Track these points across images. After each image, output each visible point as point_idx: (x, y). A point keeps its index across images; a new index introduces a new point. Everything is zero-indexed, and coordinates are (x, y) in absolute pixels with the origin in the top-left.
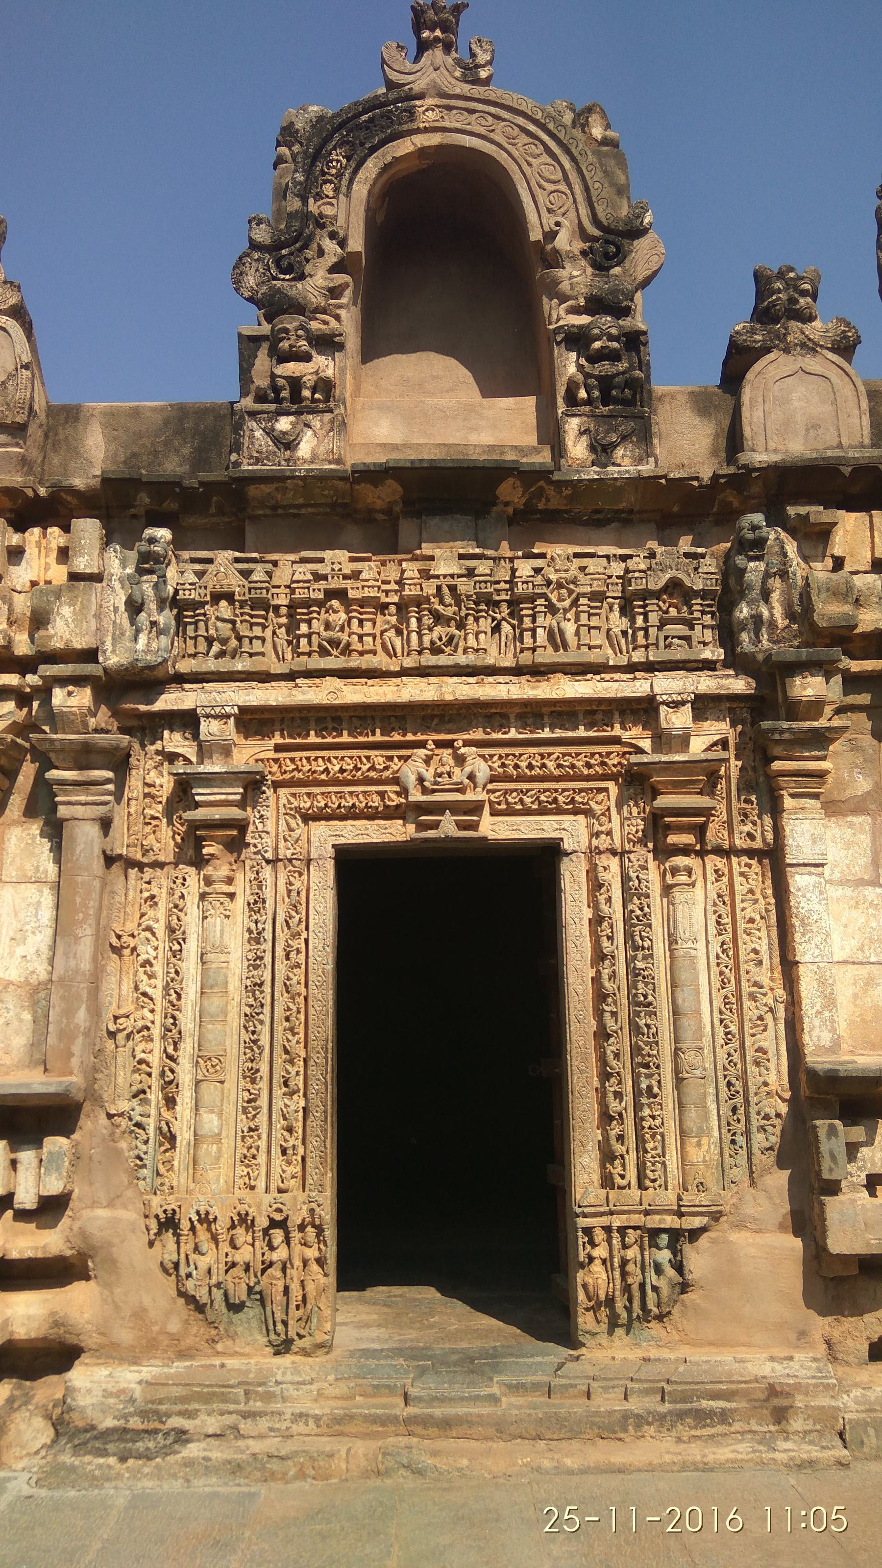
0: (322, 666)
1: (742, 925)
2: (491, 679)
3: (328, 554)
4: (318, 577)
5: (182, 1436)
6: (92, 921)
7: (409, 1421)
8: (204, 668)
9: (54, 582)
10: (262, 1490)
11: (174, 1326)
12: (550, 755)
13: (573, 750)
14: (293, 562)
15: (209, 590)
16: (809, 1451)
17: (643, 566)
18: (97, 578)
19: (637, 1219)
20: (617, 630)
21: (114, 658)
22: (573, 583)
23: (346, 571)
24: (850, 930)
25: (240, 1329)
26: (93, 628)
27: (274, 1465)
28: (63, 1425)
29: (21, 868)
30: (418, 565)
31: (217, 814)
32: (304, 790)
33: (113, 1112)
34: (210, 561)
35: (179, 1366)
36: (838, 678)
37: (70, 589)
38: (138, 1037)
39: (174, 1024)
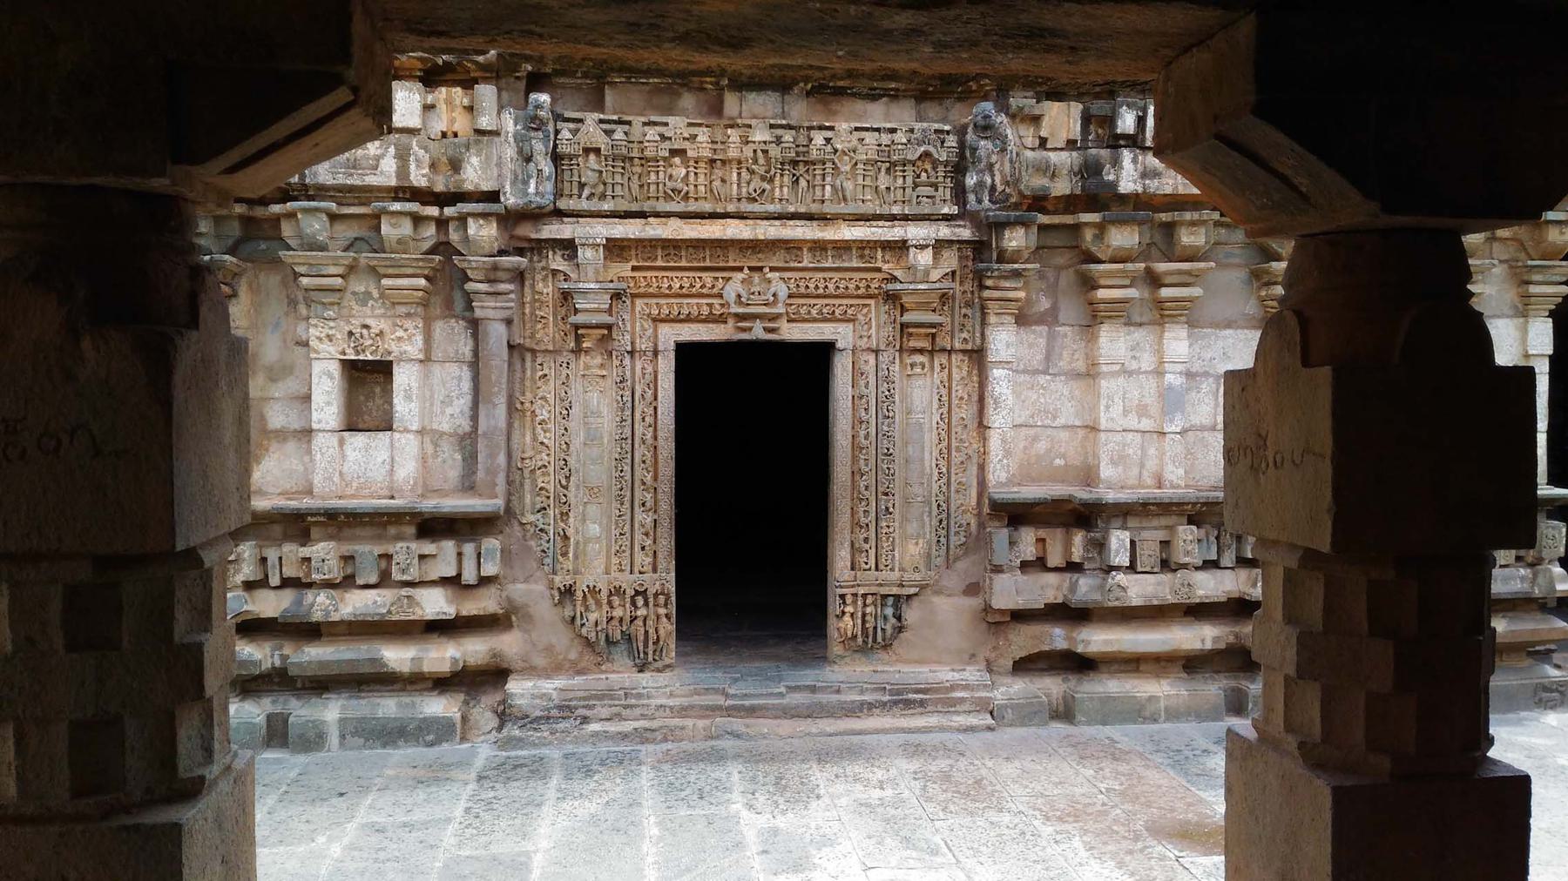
1: (955, 402)
3: (670, 120)
4: (663, 138)
5: (585, 720)
6: (504, 393)
7: (727, 709)
8: (579, 207)
11: (573, 655)
13: (848, 275)
16: (973, 720)
18: (496, 133)
19: (874, 590)
21: (511, 199)
28: (504, 716)
29: (445, 351)
30: (740, 132)
31: (595, 319)
32: (654, 301)
34: (581, 121)
36: (1035, 229)
37: (477, 142)
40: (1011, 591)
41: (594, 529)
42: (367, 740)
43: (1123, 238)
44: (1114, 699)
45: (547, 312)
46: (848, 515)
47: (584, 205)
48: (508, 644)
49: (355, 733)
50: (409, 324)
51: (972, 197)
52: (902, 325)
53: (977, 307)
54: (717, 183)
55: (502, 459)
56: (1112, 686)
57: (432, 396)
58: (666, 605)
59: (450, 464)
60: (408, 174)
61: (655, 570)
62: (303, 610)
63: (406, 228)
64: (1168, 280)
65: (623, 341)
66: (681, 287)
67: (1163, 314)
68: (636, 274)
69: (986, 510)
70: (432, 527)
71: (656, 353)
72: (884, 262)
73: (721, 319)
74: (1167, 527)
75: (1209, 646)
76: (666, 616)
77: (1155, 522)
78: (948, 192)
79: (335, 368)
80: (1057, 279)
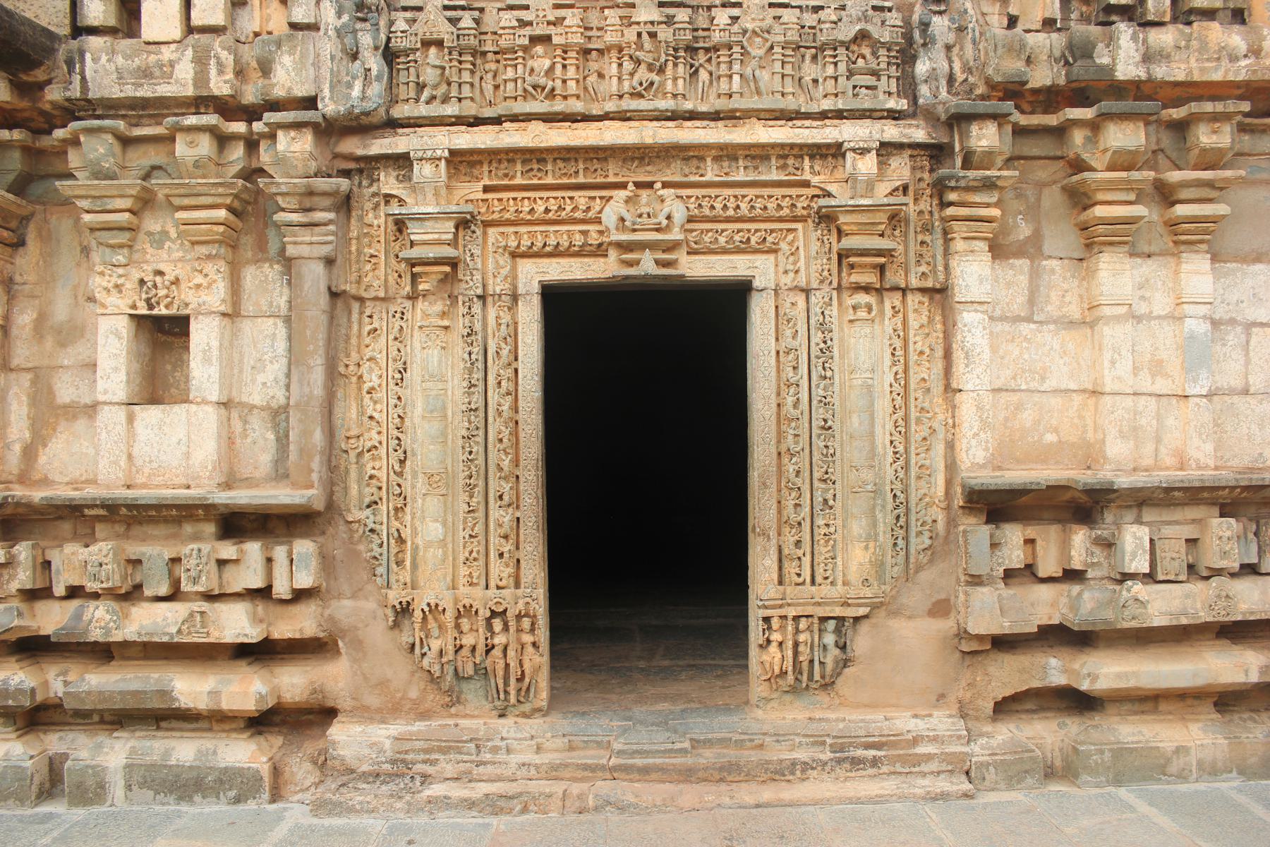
0: (528, 110)
1: (913, 357)
2: (689, 124)
4: (523, 24)
5: (425, 777)
9: (276, 33)
10: (494, 821)
12: (744, 197)
14: (499, 10)
15: (419, 38)
16: (943, 784)
17: (834, 18)
18: (314, 27)
20: (808, 79)
21: (328, 107)
22: (768, 32)
23: (551, 18)
24: (1006, 361)
25: (470, 697)
26: (312, 77)
27: (501, 803)
31: (431, 252)
32: (512, 229)
33: (350, 519)
35: (419, 726)
36: (1009, 128)
37: (290, 37)
38: (367, 455)
39: (399, 445)
40: (989, 611)
41: (433, 530)
42: (157, 793)
43: (1125, 137)
44: (1131, 750)
45: (379, 249)
46: (774, 511)
47: (423, 110)
48: (331, 677)
49: (142, 785)
50: (210, 268)
51: (924, 90)
52: (840, 256)
53: (939, 230)
54: (593, 78)
55: (318, 437)
56: (1130, 731)
57: (241, 361)
58: (532, 630)
59: (259, 448)
60: (208, 80)
61: (517, 586)
62: (82, 625)
63: (205, 145)
64: (1184, 194)
65: (470, 285)
66: (547, 211)
67: (1182, 237)
68: (489, 196)
69: (959, 501)
70: (236, 524)
71: (515, 297)
72: (813, 173)
73: (599, 251)
74: (1194, 521)
75: (1254, 678)
76: (534, 644)
77: (1178, 514)
78: (893, 82)
79: (123, 325)
80: (1039, 200)
